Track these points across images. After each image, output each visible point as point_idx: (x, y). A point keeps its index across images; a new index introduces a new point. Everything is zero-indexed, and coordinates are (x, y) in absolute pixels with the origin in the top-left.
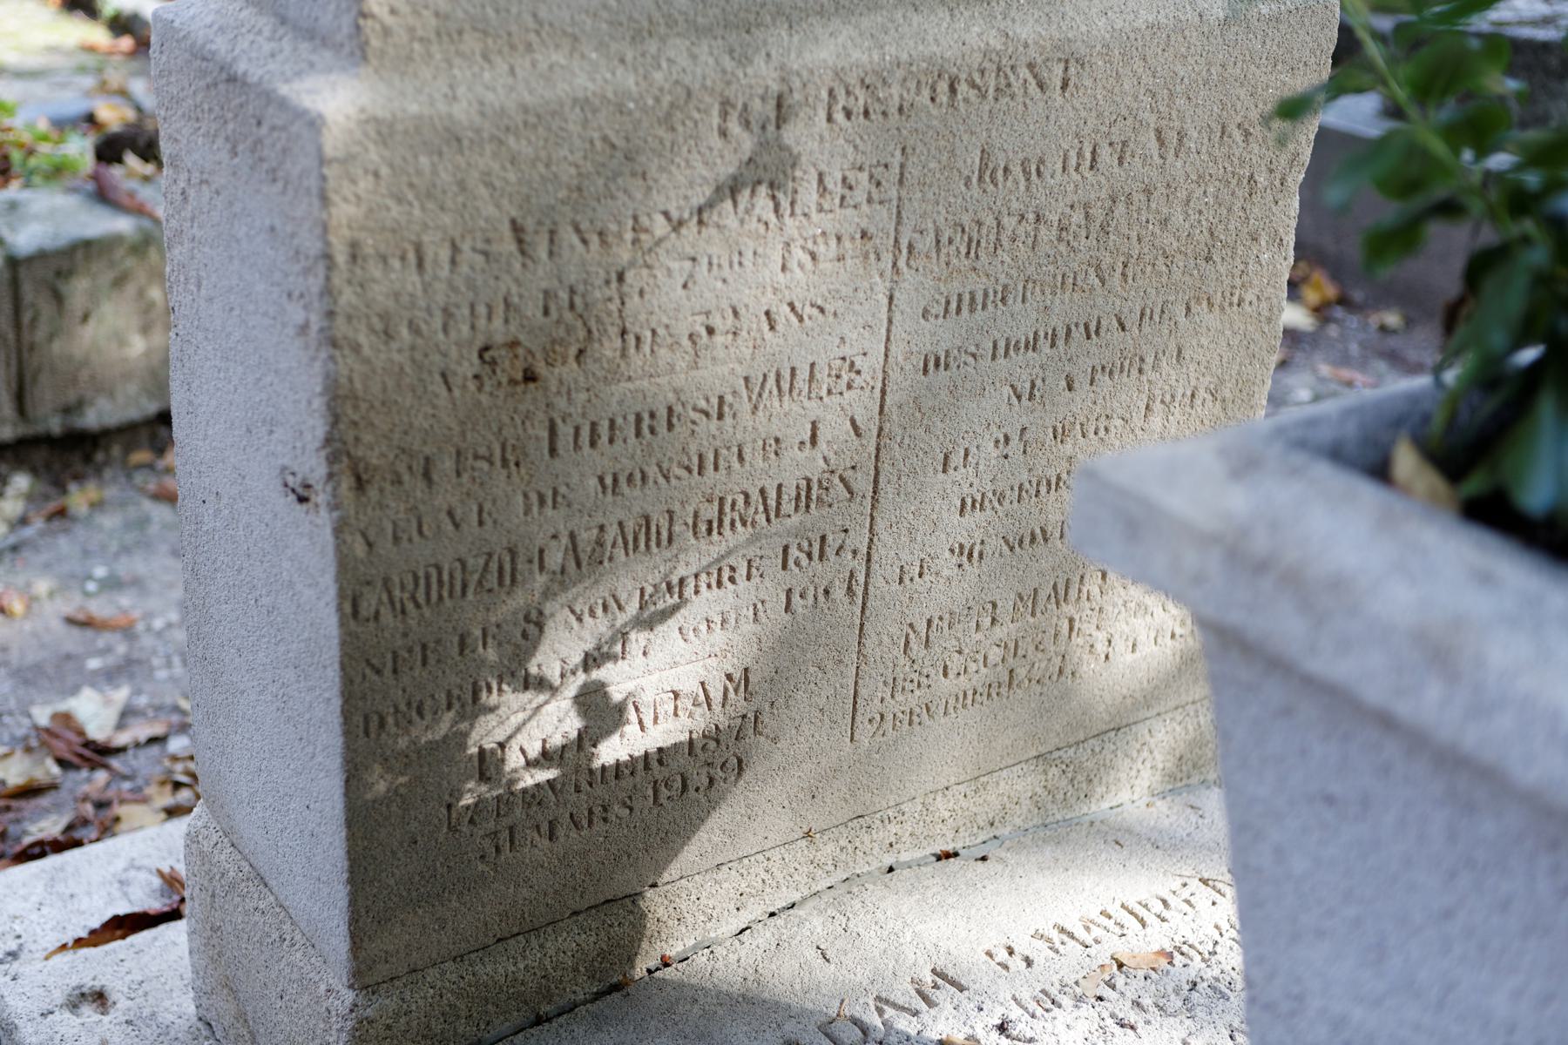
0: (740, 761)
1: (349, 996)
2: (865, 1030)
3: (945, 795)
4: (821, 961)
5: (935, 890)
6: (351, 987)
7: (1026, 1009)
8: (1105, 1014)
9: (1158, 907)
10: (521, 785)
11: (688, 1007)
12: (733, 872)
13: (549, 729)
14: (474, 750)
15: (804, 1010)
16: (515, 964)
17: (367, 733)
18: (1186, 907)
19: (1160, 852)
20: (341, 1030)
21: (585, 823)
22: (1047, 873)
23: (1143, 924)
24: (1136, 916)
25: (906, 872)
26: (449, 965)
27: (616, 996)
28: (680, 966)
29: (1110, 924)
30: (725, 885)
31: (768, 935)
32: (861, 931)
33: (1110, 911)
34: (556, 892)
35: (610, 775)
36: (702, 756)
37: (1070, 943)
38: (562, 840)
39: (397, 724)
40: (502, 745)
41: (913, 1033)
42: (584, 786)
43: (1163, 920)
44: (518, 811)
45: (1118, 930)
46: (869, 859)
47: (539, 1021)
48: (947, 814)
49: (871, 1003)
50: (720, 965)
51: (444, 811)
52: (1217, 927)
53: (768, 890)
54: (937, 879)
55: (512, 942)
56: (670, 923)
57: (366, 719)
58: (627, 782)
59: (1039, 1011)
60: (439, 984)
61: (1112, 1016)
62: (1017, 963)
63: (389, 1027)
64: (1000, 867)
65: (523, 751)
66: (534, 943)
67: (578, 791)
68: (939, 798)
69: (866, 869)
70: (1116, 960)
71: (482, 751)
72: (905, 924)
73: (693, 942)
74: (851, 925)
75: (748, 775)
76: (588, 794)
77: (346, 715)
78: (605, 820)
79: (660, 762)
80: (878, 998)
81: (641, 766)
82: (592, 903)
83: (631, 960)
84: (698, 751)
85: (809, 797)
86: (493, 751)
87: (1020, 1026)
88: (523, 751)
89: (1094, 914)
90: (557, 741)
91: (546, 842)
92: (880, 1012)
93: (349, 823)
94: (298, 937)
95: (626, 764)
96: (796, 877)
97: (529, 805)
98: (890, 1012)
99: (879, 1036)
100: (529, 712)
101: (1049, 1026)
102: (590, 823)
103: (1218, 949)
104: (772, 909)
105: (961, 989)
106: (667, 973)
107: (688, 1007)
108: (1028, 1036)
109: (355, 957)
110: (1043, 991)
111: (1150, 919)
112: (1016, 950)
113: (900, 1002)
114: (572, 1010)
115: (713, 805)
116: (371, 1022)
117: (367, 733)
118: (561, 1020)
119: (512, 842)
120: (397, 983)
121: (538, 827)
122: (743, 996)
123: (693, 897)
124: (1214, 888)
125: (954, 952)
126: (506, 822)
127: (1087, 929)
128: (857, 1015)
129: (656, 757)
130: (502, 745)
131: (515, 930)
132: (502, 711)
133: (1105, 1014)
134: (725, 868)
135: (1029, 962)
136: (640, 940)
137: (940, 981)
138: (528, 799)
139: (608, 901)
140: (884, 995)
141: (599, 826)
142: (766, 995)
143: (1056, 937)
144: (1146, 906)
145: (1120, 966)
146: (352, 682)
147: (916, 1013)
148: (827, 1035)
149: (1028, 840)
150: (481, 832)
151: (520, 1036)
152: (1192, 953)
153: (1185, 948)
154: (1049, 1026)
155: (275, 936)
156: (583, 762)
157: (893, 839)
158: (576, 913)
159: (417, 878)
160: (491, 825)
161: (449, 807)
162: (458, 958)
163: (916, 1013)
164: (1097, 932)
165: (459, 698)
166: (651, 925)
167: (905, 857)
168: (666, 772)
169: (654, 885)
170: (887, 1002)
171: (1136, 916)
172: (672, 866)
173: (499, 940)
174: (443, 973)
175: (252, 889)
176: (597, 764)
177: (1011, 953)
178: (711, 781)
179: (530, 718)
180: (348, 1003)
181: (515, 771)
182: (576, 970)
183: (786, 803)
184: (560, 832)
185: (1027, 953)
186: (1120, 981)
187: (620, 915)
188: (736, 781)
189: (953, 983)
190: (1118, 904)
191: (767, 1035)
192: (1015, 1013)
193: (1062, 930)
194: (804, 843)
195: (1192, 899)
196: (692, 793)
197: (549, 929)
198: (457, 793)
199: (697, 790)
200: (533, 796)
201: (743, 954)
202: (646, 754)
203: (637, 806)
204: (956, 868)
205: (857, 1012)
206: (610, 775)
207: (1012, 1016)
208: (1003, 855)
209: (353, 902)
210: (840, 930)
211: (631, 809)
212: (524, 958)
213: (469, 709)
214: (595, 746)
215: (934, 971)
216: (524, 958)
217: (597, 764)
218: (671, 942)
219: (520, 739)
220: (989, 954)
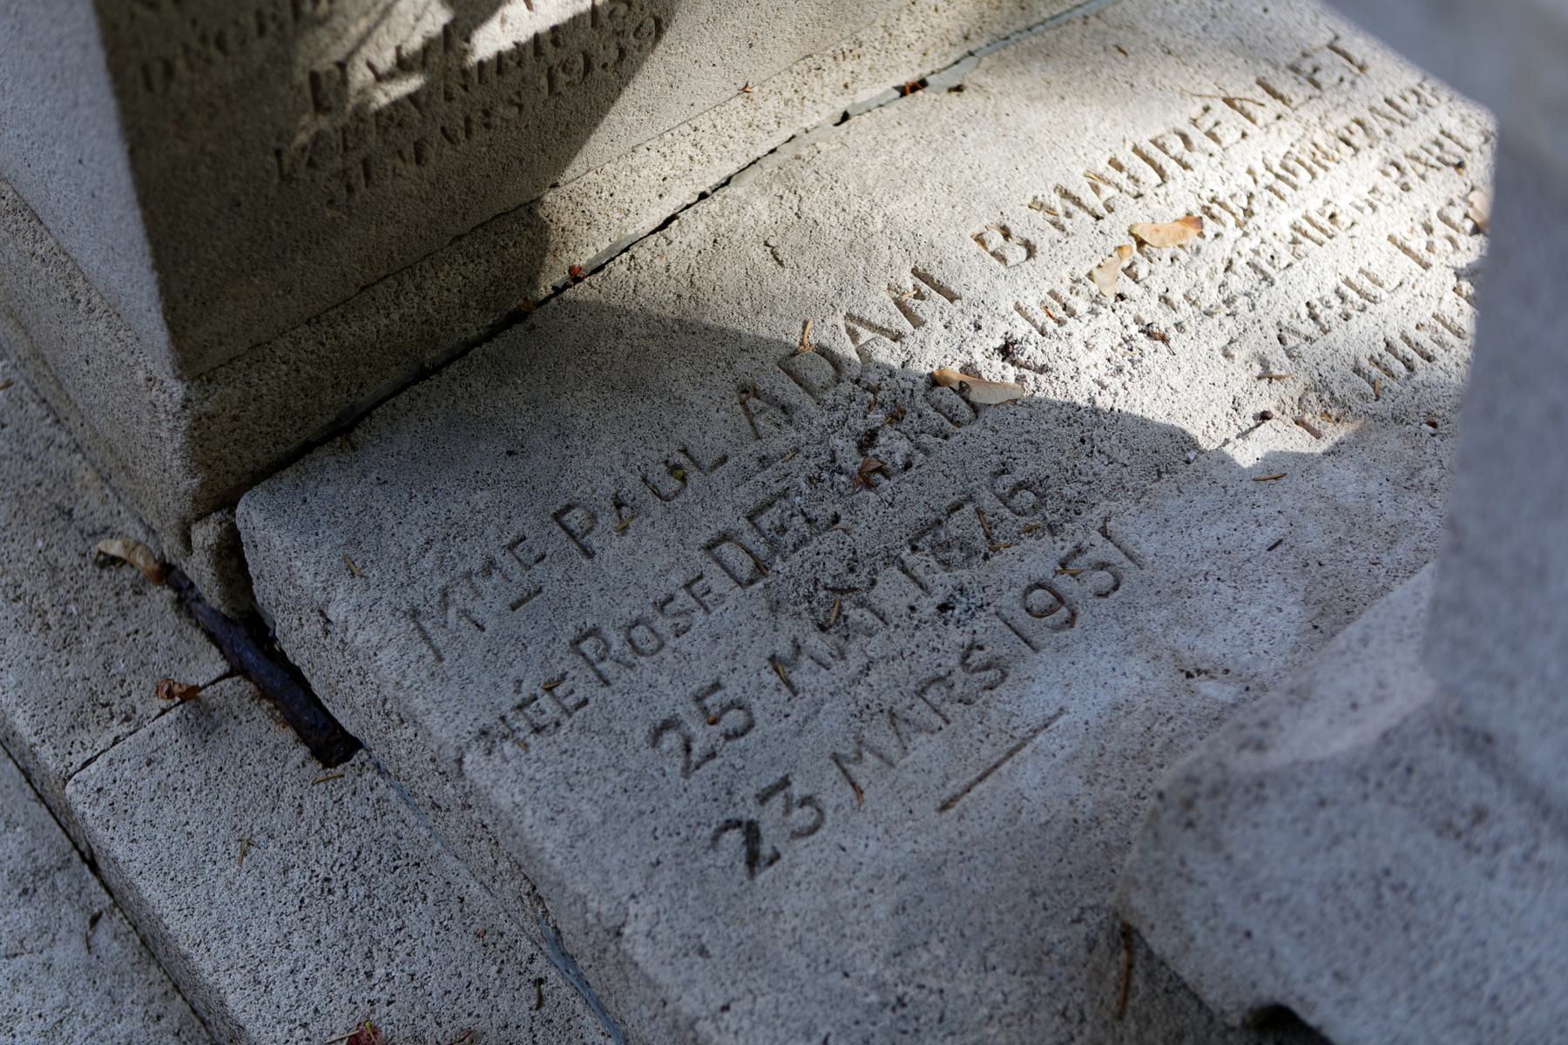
0: (658, 22)
1: (178, 390)
2: (836, 363)
3: (911, 12)
4: (771, 264)
5: (904, 145)
6: (179, 378)
7: (1033, 322)
8: (1129, 320)
9: (1177, 146)
10: (374, 106)
11: (611, 343)
12: (653, 153)
13: (403, 32)
14: (302, 78)
15: (758, 339)
16: (388, 316)
17: (149, 86)
18: (1211, 145)
19: (1171, 60)
20: (175, 429)
21: (461, 135)
22: (1039, 105)
23: (1160, 171)
24: (1152, 163)
25: (865, 118)
26: (303, 330)
27: (519, 329)
28: (594, 279)
29: (1121, 178)
30: (644, 172)
31: (701, 227)
32: (818, 215)
33: (1121, 159)
34: (430, 221)
35: (491, 73)
36: (609, 26)
37: (1080, 214)
38: (433, 161)
39: (191, 67)
40: (342, 66)
41: (896, 365)
42: (458, 91)
43: (1186, 166)
44: (372, 139)
45: (1132, 189)
46: (818, 107)
47: (423, 374)
48: (914, 36)
49: (841, 323)
50: (644, 276)
51: (272, 159)
52: (1250, 172)
53: (697, 167)
54: (905, 128)
55: (380, 287)
56: (579, 229)
57: (146, 70)
58: (512, 78)
59: (1051, 325)
60: (293, 357)
61: (1137, 320)
62: (1017, 254)
63: (235, 418)
64: (979, 101)
65: (371, 66)
66: (409, 285)
67: (449, 97)
68: (904, 17)
69: (816, 120)
70: (1136, 237)
71: (314, 77)
72: (874, 204)
73: (607, 244)
74: (805, 209)
75: (669, 36)
76: (463, 101)
77: (116, 70)
78: (487, 126)
79: (555, 42)
80: (849, 316)
81: (530, 53)
82: (478, 222)
83: (532, 281)
84: (604, 21)
85: (745, 47)
86: (329, 74)
87: (1030, 349)
88: (371, 66)
89: (1102, 166)
90: (415, 43)
91: (413, 167)
92: (854, 335)
93: (144, 201)
94: (96, 300)
95: (510, 55)
96: (731, 146)
97: (386, 129)
98: (865, 335)
99: (856, 373)
100: (374, 16)
101: (1063, 346)
102: (468, 132)
103: (1256, 207)
104: (701, 189)
105: (952, 297)
106: (581, 292)
107: (611, 343)
108: (1039, 362)
109: (179, 348)
110: (1053, 294)
111: (1171, 167)
112: (1013, 232)
113: (877, 321)
114: (464, 353)
115: (625, 80)
116: (211, 417)
117: (149, 86)
118: (453, 369)
119: (367, 176)
120: (238, 364)
121: (400, 153)
122: (679, 321)
123: (605, 194)
124: (1242, 111)
125: (939, 243)
126: (356, 156)
127: (1096, 189)
128: (825, 343)
129: (549, 38)
130: (342, 66)
131: (382, 273)
132: (337, 21)
133: (1129, 320)
134: (642, 149)
135: (1031, 250)
136: (543, 256)
137: (925, 288)
138: (384, 121)
139: (497, 216)
140: (856, 312)
141: (479, 135)
142: (708, 320)
143: (1056, 201)
144: (1162, 148)
145: (1141, 243)
146: (115, 27)
147: (897, 337)
148: (789, 373)
149: (1008, 54)
150: (325, 174)
151: (404, 396)
152: (1226, 216)
153: (1215, 209)
154: (1063, 346)
155: (66, 294)
156: (453, 62)
157: (848, 80)
158: (459, 238)
159: (247, 244)
160: (338, 163)
161: (278, 153)
162: (313, 320)
163: (897, 337)
164: (1108, 191)
165: (274, 17)
166: (555, 238)
167: (863, 96)
168: (563, 54)
169: (555, 186)
170: (861, 321)
171: (1152, 163)
172: (576, 160)
173: (363, 289)
174: (296, 343)
175: (24, 225)
176: (473, 60)
177: (1007, 235)
178: (622, 52)
179: (377, 24)
180: (178, 397)
181: (362, 91)
182: (465, 305)
183: (717, 60)
184: (430, 153)
185: (1026, 235)
186: (1142, 269)
187: (519, 227)
188: (654, 45)
189: (940, 289)
190: (1129, 146)
191: (716, 380)
192: (1021, 329)
193: (1066, 194)
194: (740, 101)
195: (1217, 130)
196: (598, 70)
197: (426, 264)
198: (285, 135)
199: (605, 66)
200: (391, 118)
201: (672, 257)
202: (537, 36)
203: (527, 102)
204: (926, 108)
205: (825, 337)
206: (491, 73)
207: (1018, 336)
208: (982, 80)
209: (165, 290)
210: (791, 214)
211: (520, 107)
212: (398, 305)
213: (289, 29)
214: (468, 40)
215: (915, 271)
216: (398, 305)
217: (473, 60)
218: (580, 250)
219: (367, 52)
220: (979, 239)
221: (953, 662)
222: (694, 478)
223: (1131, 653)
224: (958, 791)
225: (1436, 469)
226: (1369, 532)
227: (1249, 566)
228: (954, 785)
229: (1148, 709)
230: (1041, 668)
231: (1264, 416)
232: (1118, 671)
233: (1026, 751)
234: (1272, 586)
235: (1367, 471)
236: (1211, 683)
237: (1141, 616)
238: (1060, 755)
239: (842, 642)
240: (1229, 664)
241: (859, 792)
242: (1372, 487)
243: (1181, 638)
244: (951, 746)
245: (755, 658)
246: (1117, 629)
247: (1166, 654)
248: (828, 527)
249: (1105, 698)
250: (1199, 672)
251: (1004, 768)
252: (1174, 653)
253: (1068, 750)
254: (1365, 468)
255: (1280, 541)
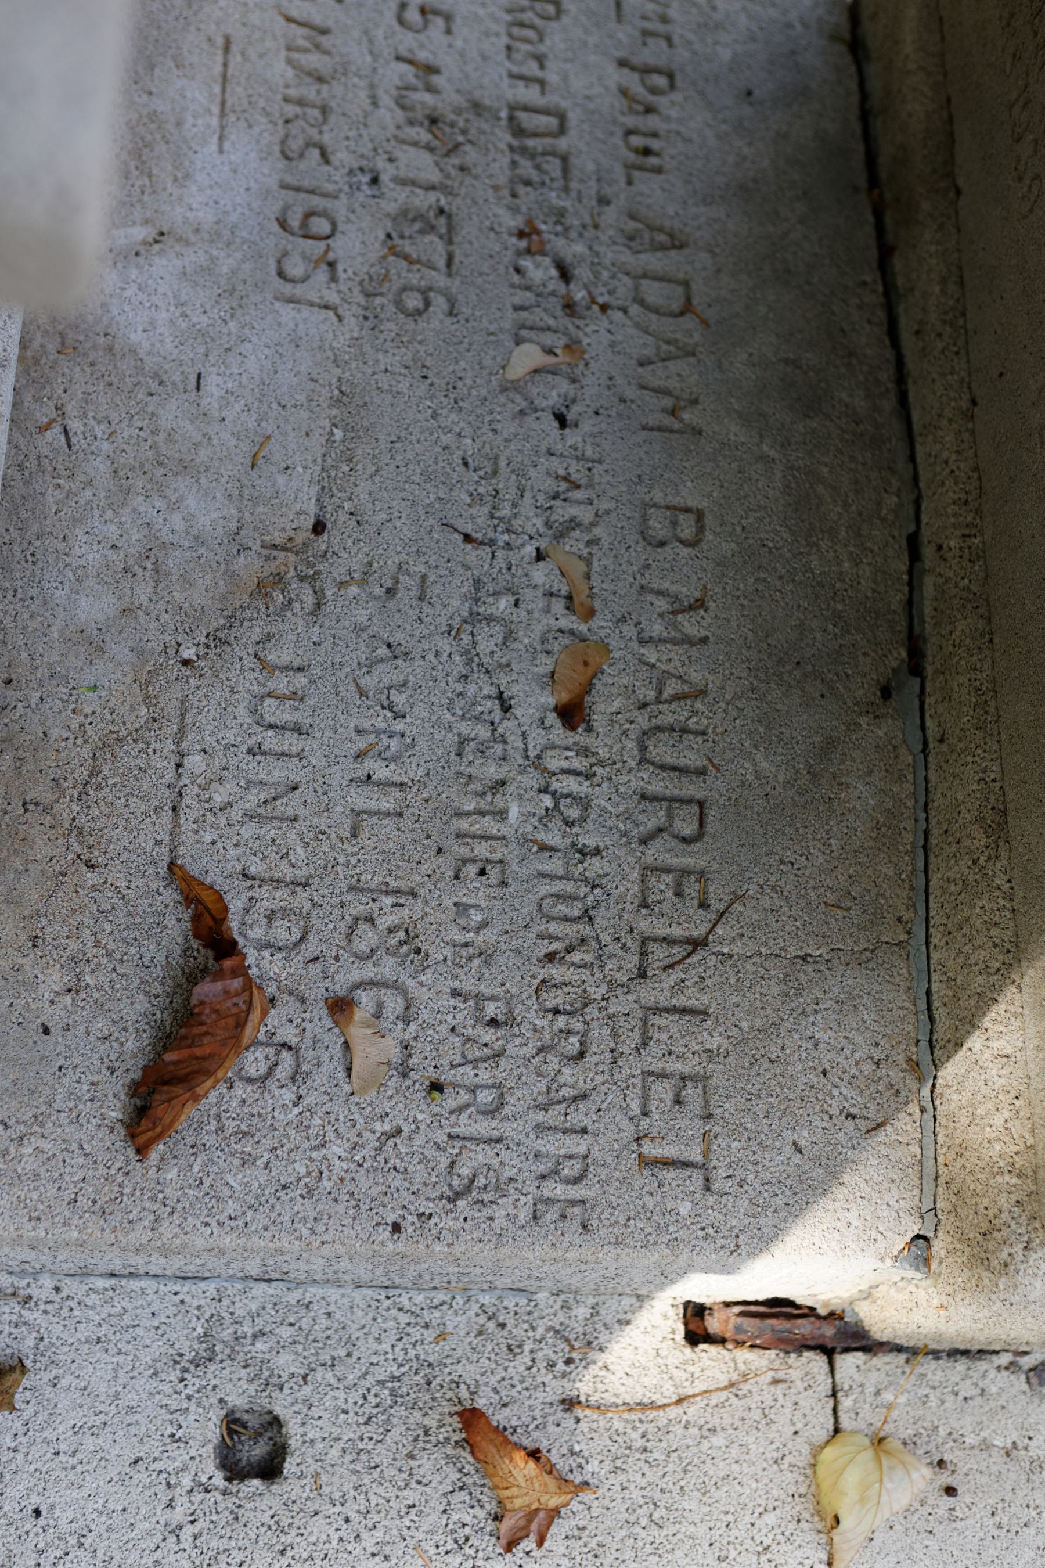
221: (326, 139)
222: (632, 157)
223: (217, 223)
224: (230, 57)
225: (144, 599)
226: (142, 466)
227: (202, 350)
228: (235, 59)
229: (164, 189)
230: (266, 171)
231: (319, 528)
232: (211, 203)
233: (216, 110)
234: (169, 345)
235: (196, 538)
236: (141, 237)
237: (239, 255)
238: (190, 120)
239: (411, 114)
240: (141, 260)
241: (289, 20)
242: (177, 521)
243: (195, 257)
244: (266, 81)
245: (445, 60)
246: (244, 234)
247: (193, 238)
248: (676, 837)
249: (201, 178)
250: (157, 242)
251: (217, 89)
252: (188, 243)
253: (187, 126)
254: (199, 540)
255: (198, 389)
